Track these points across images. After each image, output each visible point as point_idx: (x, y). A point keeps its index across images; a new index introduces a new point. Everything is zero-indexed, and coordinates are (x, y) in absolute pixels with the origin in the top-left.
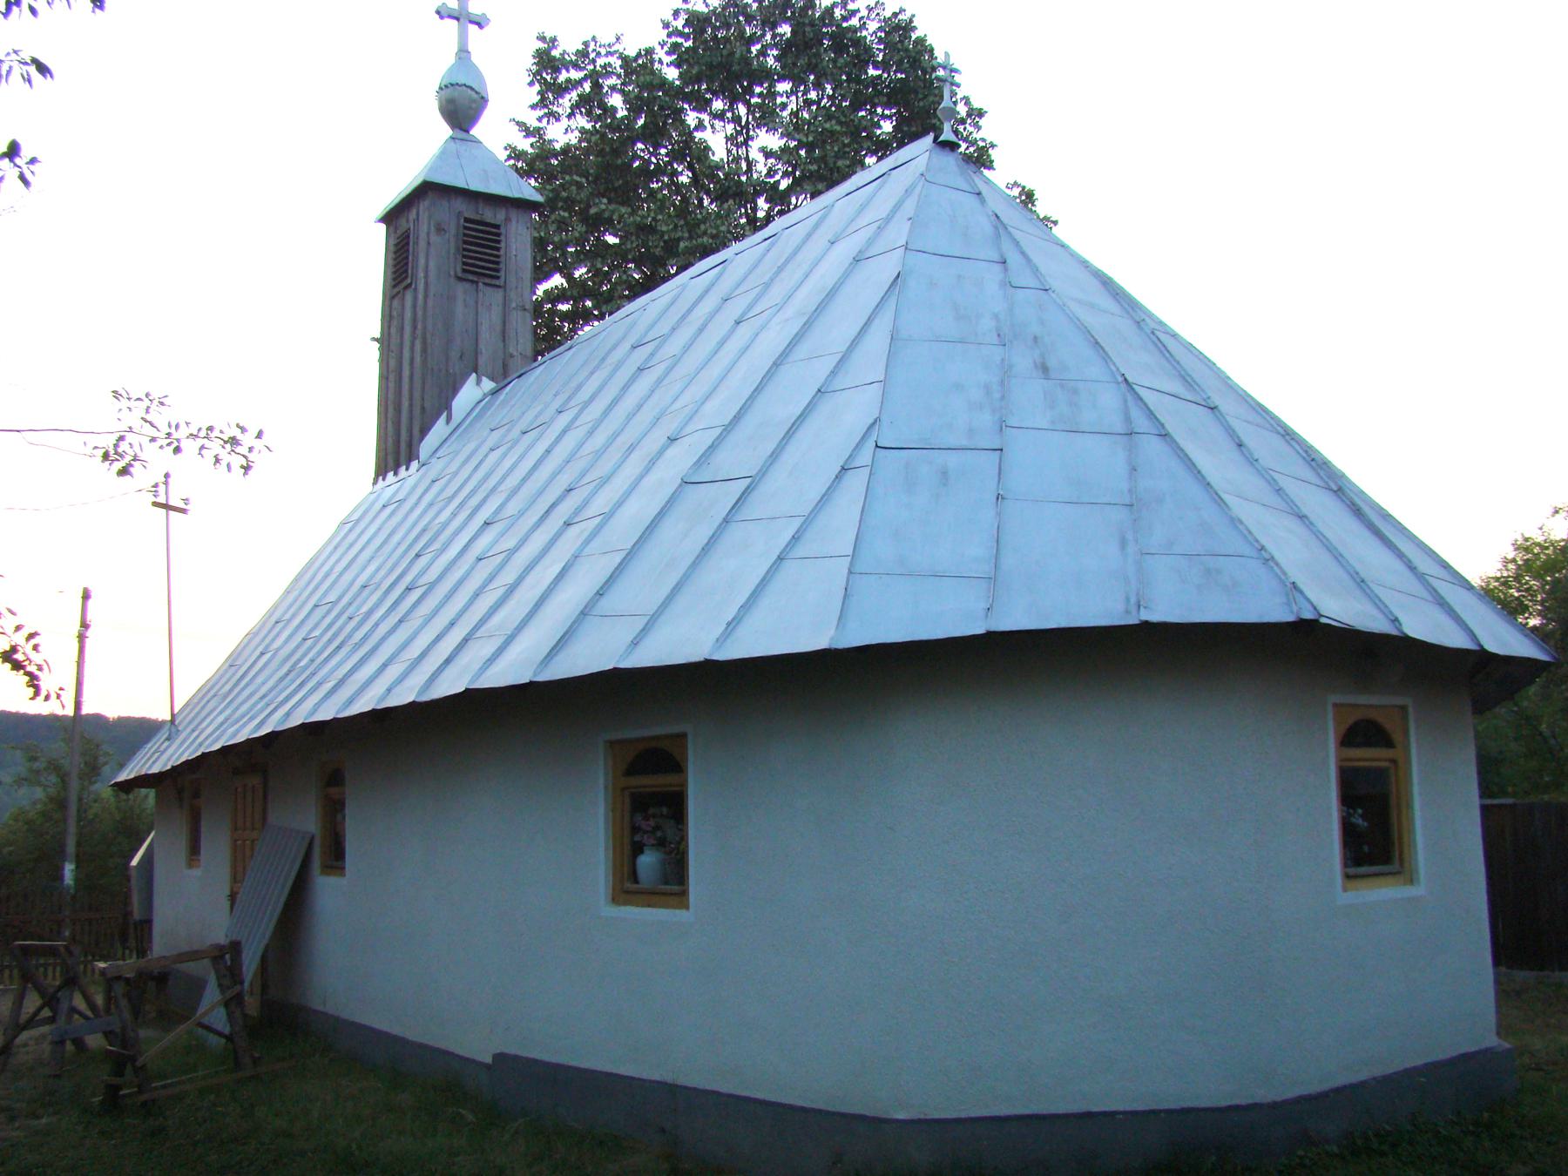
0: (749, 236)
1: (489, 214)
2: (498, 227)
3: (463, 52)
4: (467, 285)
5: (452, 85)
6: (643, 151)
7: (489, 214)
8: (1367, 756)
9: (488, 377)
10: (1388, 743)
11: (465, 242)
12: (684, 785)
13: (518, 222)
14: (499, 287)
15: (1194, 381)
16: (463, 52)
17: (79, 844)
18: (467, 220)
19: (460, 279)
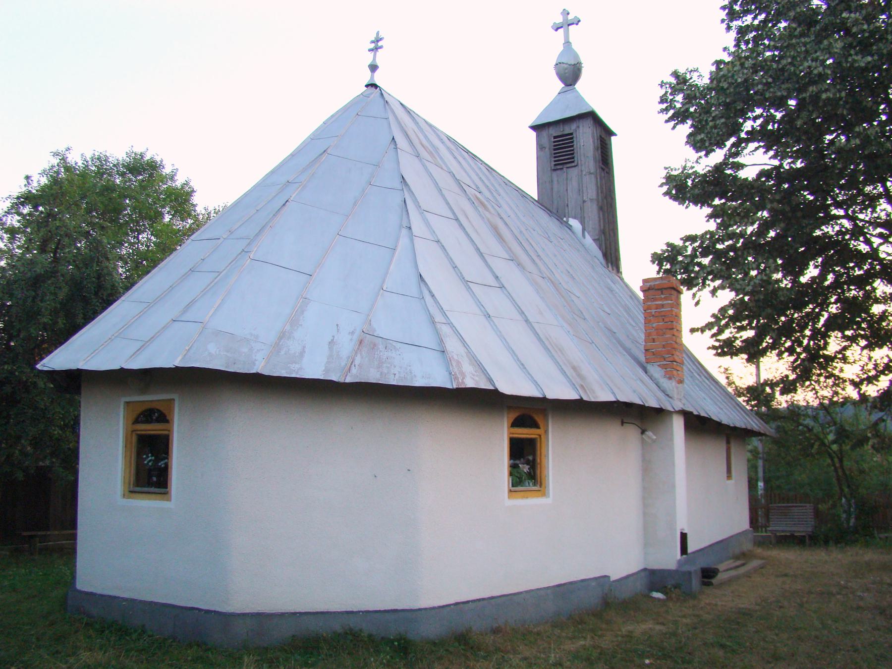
0: (162, 260)
1: (567, 130)
2: (571, 134)
3: (567, 43)
4: (558, 172)
5: (560, 63)
6: (755, 18)
7: (567, 130)
8: (524, 433)
9: (573, 218)
10: (167, 421)
11: (555, 150)
12: (170, 430)
13: (583, 126)
14: (575, 166)
15: (205, 289)
16: (567, 43)
17: (764, 472)
18: (555, 137)
19: (554, 170)
